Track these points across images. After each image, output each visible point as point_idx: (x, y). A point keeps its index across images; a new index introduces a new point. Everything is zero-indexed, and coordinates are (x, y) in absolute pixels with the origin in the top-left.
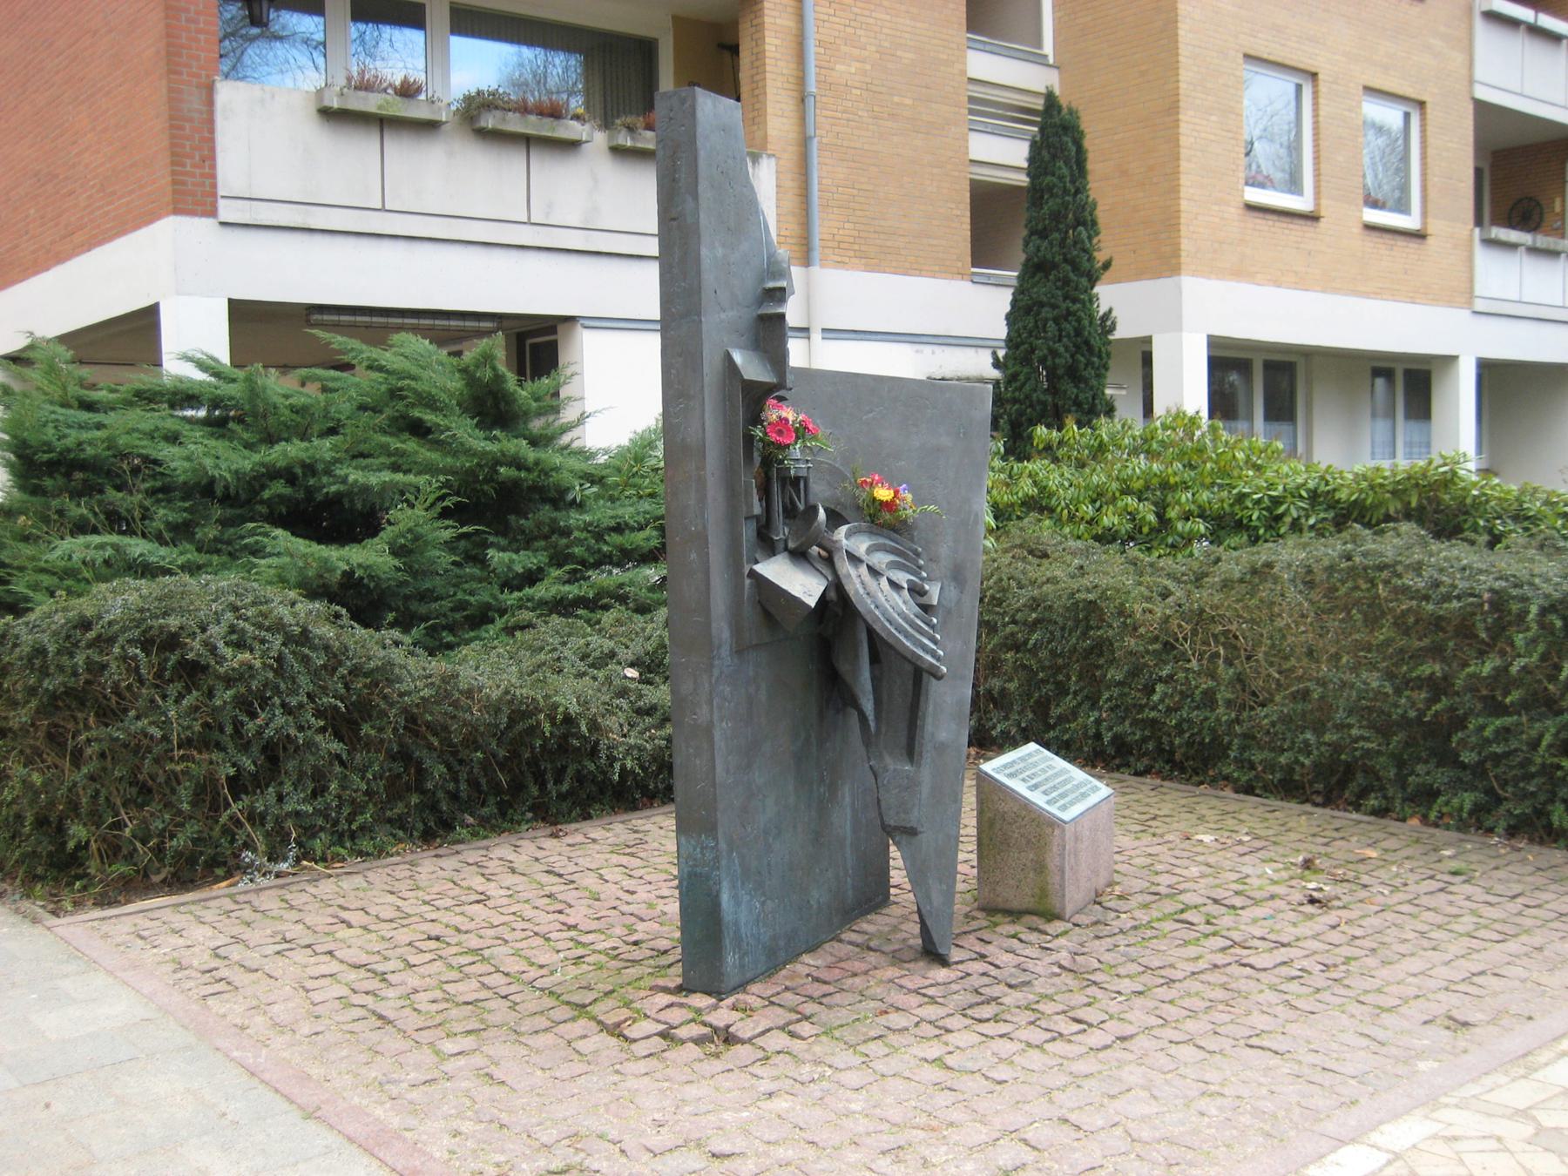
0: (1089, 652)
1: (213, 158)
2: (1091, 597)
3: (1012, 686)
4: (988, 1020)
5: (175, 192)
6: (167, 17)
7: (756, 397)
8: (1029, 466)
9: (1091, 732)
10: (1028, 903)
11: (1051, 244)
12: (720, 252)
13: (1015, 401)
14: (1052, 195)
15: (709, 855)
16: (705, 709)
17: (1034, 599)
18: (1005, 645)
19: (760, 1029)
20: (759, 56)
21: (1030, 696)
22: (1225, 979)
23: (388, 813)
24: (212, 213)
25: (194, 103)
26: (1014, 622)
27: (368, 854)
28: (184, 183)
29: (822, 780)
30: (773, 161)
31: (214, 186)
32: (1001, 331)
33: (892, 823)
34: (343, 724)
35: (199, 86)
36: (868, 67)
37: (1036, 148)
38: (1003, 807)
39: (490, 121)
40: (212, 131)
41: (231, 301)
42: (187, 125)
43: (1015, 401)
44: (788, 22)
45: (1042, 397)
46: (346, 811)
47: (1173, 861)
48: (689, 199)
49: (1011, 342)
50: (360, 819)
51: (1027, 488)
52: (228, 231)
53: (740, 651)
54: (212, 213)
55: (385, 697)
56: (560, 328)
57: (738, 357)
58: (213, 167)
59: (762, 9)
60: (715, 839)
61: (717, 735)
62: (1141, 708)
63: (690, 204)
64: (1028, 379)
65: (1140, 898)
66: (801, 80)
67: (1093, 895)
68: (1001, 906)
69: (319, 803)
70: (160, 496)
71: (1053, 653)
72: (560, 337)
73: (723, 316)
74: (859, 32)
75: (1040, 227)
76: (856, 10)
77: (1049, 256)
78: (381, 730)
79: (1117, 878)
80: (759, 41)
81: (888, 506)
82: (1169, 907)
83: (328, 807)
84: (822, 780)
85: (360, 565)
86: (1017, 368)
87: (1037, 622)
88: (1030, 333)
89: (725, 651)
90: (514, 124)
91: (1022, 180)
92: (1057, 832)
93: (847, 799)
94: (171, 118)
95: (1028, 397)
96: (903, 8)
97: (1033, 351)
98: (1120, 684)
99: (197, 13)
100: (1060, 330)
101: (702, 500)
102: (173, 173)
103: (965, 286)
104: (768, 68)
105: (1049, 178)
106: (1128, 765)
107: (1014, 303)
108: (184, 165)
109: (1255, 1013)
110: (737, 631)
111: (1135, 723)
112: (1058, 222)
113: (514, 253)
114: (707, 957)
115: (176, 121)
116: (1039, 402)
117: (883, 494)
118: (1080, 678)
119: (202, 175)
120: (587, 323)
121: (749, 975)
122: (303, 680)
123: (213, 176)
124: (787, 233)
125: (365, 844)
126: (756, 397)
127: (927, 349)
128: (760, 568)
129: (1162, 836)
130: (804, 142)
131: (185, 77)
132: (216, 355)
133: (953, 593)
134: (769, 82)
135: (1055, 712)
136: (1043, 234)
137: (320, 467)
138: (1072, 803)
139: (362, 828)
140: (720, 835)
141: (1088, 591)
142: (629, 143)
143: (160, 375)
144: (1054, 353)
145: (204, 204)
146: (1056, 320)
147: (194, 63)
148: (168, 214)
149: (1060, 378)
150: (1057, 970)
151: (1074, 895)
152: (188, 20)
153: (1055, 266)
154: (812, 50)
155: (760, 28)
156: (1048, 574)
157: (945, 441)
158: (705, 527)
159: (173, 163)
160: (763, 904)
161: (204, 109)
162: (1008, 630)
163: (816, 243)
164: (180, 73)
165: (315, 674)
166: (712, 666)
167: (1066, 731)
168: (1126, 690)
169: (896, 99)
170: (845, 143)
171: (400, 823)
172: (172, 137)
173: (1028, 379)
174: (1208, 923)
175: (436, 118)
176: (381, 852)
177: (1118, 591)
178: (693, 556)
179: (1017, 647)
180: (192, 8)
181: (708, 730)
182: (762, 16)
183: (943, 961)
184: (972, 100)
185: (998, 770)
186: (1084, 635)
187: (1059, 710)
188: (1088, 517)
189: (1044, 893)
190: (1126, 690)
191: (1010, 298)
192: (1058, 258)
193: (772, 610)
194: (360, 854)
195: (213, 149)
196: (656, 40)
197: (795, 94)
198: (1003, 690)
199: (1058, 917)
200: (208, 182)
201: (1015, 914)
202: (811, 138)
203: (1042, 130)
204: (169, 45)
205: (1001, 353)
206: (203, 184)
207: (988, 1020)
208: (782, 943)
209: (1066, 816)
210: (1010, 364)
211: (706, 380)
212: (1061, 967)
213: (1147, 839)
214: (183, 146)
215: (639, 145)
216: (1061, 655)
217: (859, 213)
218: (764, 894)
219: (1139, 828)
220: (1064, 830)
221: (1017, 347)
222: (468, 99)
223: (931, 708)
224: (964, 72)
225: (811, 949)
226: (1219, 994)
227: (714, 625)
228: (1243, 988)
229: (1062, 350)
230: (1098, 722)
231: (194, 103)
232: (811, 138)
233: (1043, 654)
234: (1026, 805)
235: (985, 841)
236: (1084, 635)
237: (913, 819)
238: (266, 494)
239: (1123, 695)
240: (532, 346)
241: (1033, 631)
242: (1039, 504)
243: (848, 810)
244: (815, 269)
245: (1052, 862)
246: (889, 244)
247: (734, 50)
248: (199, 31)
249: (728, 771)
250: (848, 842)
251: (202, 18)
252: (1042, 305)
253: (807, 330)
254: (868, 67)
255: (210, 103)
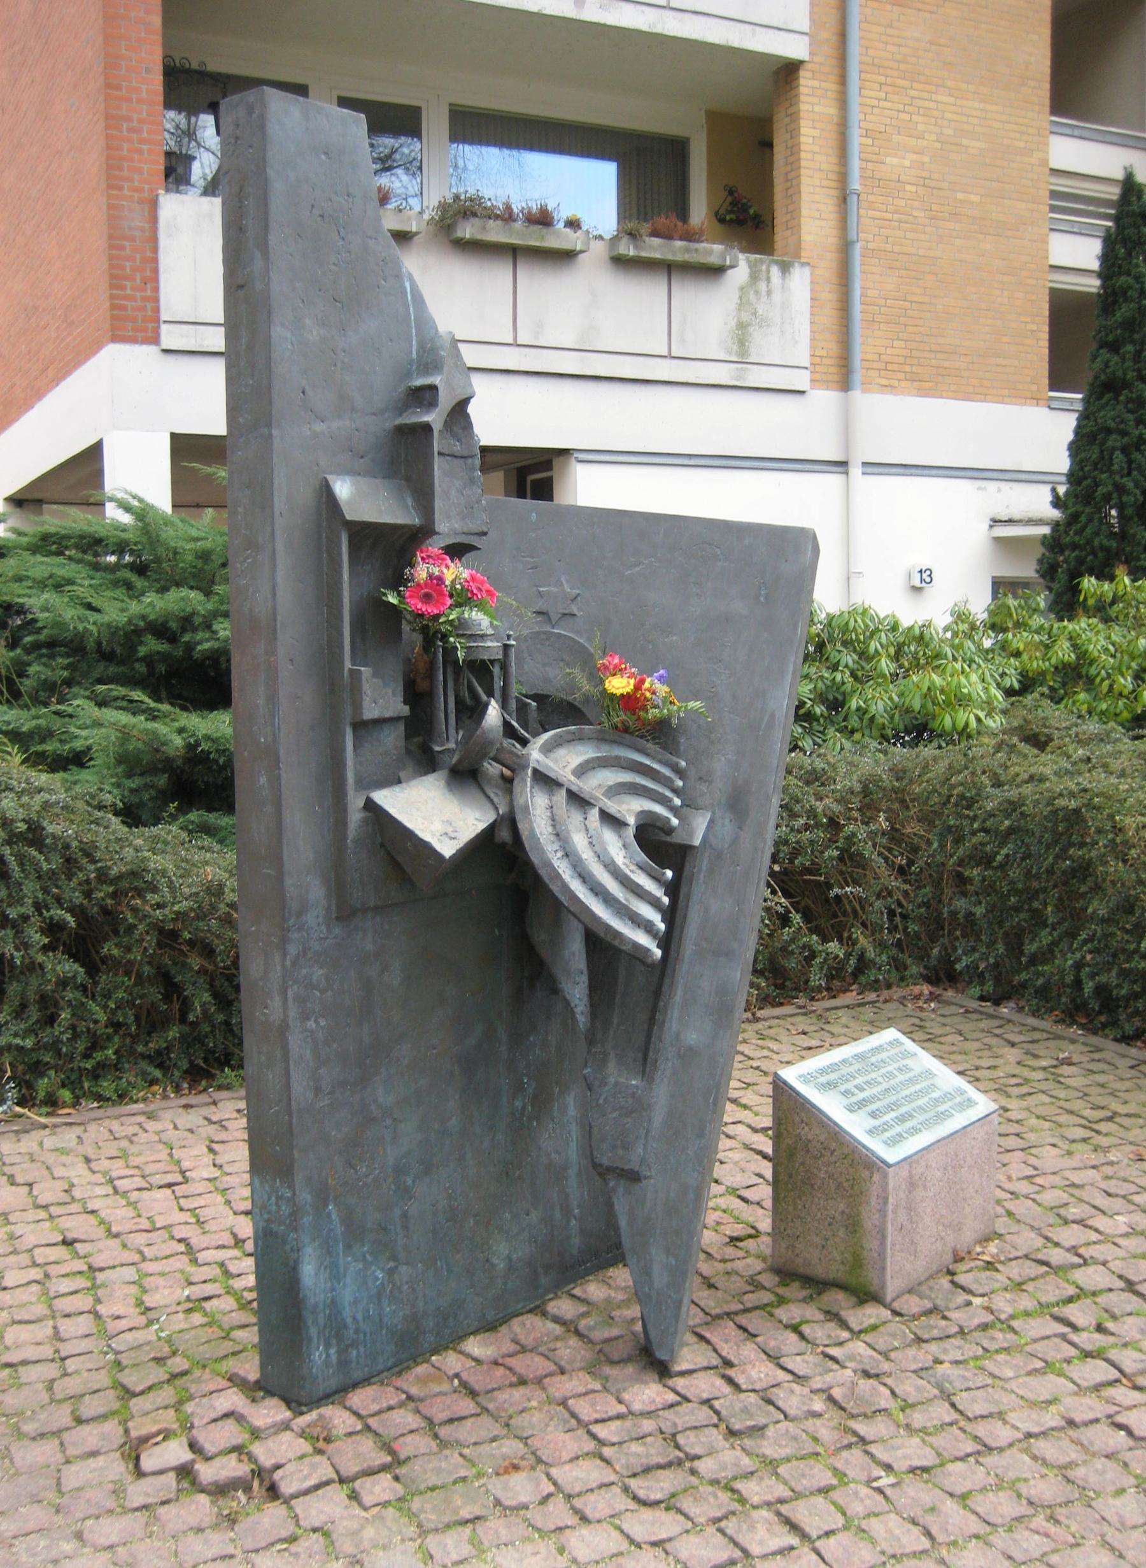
0: (1073, 872)
1: (155, 279)
2: (1073, 804)
3: (979, 911)
4: (656, 1503)
5: (113, 317)
6: (107, 127)
7: (389, 550)
8: (1070, 626)
9: (1069, 979)
10: (836, 1271)
11: (1123, 360)
12: (314, 333)
13: (1074, 546)
14: (1126, 300)
15: (285, 1210)
16: (276, 1002)
17: (1010, 803)
18: (970, 857)
19: (312, 1482)
20: (794, 150)
21: (1000, 924)
22: (1074, 1454)
23: (140, 1048)
24: (155, 340)
25: (136, 219)
26: (986, 831)
27: (108, 1099)
28: (124, 308)
29: (519, 1088)
30: (807, 271)
31: (157, 310)
32: (1062, 463)
33: (605, 1162)
34: (82, 942)
35: (141, 202)
36: (926, 159)
37: (1110, 243)
38: (805, 1132)
39: (467, 230)
40: (155, 250)
41: (174, 436)
42: (127, 244)
43: (1074, 546)
44: (830, 110)
45: (1106, 542)
46: (81, 1046)
47: (1102, 1201)
48: (258, 254)
49: (1073, 477)
50: (99, 1056)
51: (1063, 652)
52: (171, 359)
53: (344, 912)
54: (155, 340)
55: (135, 910)
56: (556, 463)
57: (343, 489)
58: (156, 289)
59: (797, 96)
60: (291, 1186)
61: (295, 1041)
62: (1129, 957)
63: (258, 263)
64: (1090, 521)
65: (1016, 1270)
66: (843, 178)
67: (949, 1257)
68: (801, 1270)
69: (46, 1036)
70: (44, 651)
71: (1028, 874)
72: (555, 473)
73: (319, 427)
74: (916, 118)
75: (1111, 338)
76: (913, 93)
77: (1120, 373)
78: (129, 949)
79: (1001, 1225)
80: (794, 133)
81: (630, 702)
82: (1052, 1290)
83: (58, 1041)
84: (519, 1088)
85: (207, 738)
86: (1079, 508)
87: (1011, 831)
88: (1095, 465)
89: (314, 918)
90: (495, 233)
91: (1093, 285)
92: (876, 1177)
93: (572, 1111)
94: (111, 237)
95: (1089, 542)
96: (971, 88)
97: (1097, 484)
98: (1103, 921)
99: (140, 121)
100: (1130, 462)
101: (272, 698)
102: (112, 297)
103: (1042, 412)
104: (803, 163)
105: (1123, 279)
106: (1114, 1024)
107: (1078, 432)
108: (124, 288)
109: (1092, 1542)
110: (338, 887)
111: (1124, 974)
112: (1133, 331)
113: (498, 378)
114: (296, 1351)
115: (115, 239)
116: (1102, 547)
117: (619, 685)
118: (1057, 909)
119: (144, 299)
120: (581, 456)
121: (357, 1375)
122: (30, 888)
123: (157, 300)
124: (824, 353)
125: (107, 1086)
126: (389, 550)
127: (992, 486)
128: (390, 800)
129: (1106, 1150)
130: (845, 248)
131: (126, 192)
132: (150, 499)
133: (726, 827)
134: (804, 180)
135: (1030, 948)
136: (1114, 347)
137: (197, 620)
138: (914, 1131)
139: (100, 1065)
140: (299, 1179)
141: (1072, 795)
142: (632, 252)
143: (104, 517)
144: (1120, 489)
145: (145, 330)
146: (1125, 450)
147: (136, 177)
148: (108, 343)
149: (1130, 518)
150: (818, 1405)
151: (901, 1266)
152: (130, 130)
153: (1126, 384)
154: (856, 140)
155: (794, 117)
156: (1033, 770)
157: (739, 607)
158: (274, 740)
159: (112, 287)
160: (391, 1272)
161: (147, 226)
162: (975, 840)
163: (857, 363)
164: (120, 188)
165: (46, 879)
166: (284, 940)
167: (1039, 974)
168: (1113, 929)
169: (960, 196)
170: (897, 249)
171: (160, 1060)
172: (111, 258)
173: (1090, 521)
174: (1100, 1328)
175: (406, 228)
176: (122, 1097)
177: (1109, 798)
178: (263, 780)
179: (986, 861)
180: (135, 116)
181: (283, 1028)
182: (797, 103)
183: (662, 1370)
184: (1054, 195)
185: (806, 1078)
186: (1062, 855)
187: (1034, 947)
188: (1126, 692)
189: (857, 1262)
190: (1113, 929)
191: (1074, 423)
192: (1131, 375)
193: (399, 859)
194: (99, 1098)
195: (156, 271)
196: (688, 139)
197: (833, 192)
198: (970, 915)
199: (866, 1295)
200: (149, 305)
201: (816, 1285)
202: (853, 242)
203: (1117, 219)
204: (109, 157)
205: (1062, 490)
206: (144, 309)
207: (656, 1503)
208: (429, 1324)
209: (891, 1155)
210: (1070, 504)
211: (279, 522)
212: (831, 1399)
213: (1084, 1154)
214: (123, 268)
215: (644, 254)
216: (1037, 877)
217: (910, 329)
218: (394, 1258)
219: (1081, 1133)
220: (885, 1176)
221: (1079, 483)
222: (443, 207)
223: (679, 995)
224: (1045, 162)
225: (489, 1327)
226: (1047, 1489)
227: (289, 882)
228: (1093, 1480)
229: (1130, 485)
230: (1079, 966)
231: (136, 219)
232: (853, 242)
233: (1014, 873)
234: (836, 1134)
235: (784, 1177)
236: (1062, 855)
237: (633, 1159)
238: (142, 651)
239: (1107, 936)
240: (534, 482)
241: (1003, 844)
242: (1075, 674)
243: (574, 1127)
244: (856, 394)
245: (870, 1219)
246: (947, 364)
247: (767, 145)
248: (142, 141)
249: (318, 1090)
250: (572, 1172)
251: (145, 127)
252: (1109, 431)
253: (843, 464)
254: (926, 159)
255: (154, 219)
